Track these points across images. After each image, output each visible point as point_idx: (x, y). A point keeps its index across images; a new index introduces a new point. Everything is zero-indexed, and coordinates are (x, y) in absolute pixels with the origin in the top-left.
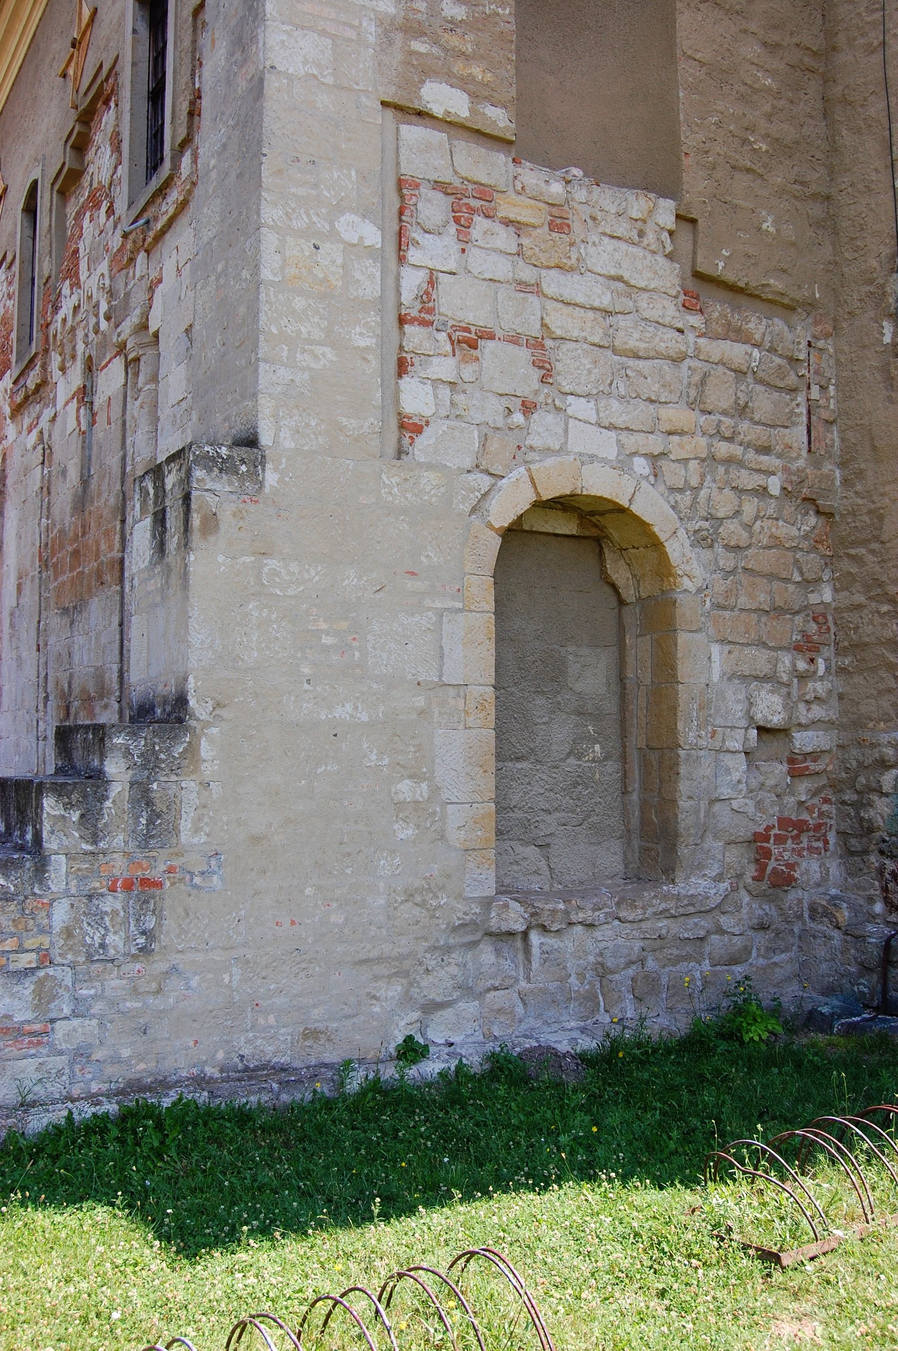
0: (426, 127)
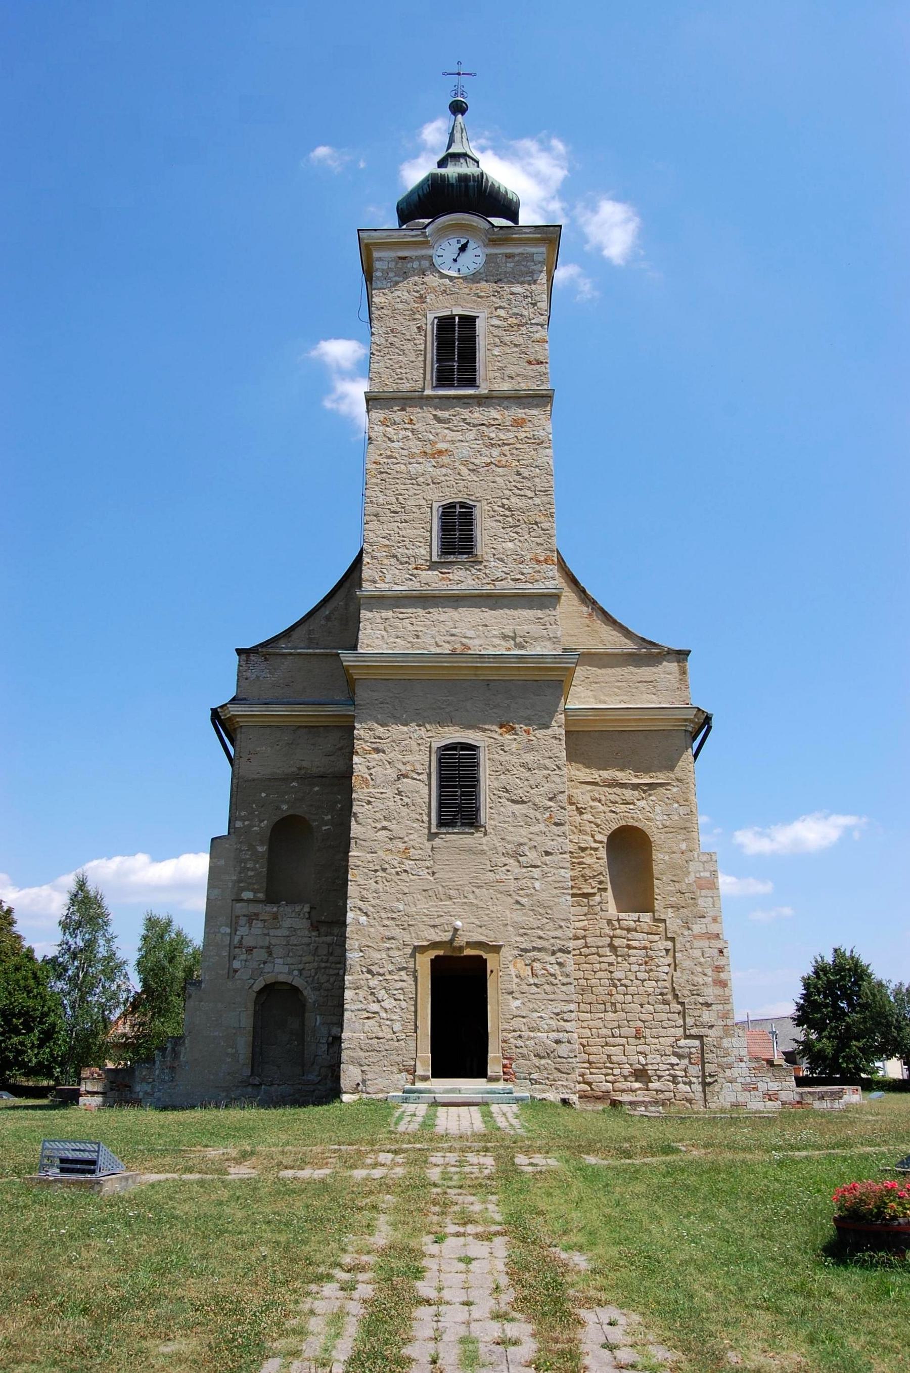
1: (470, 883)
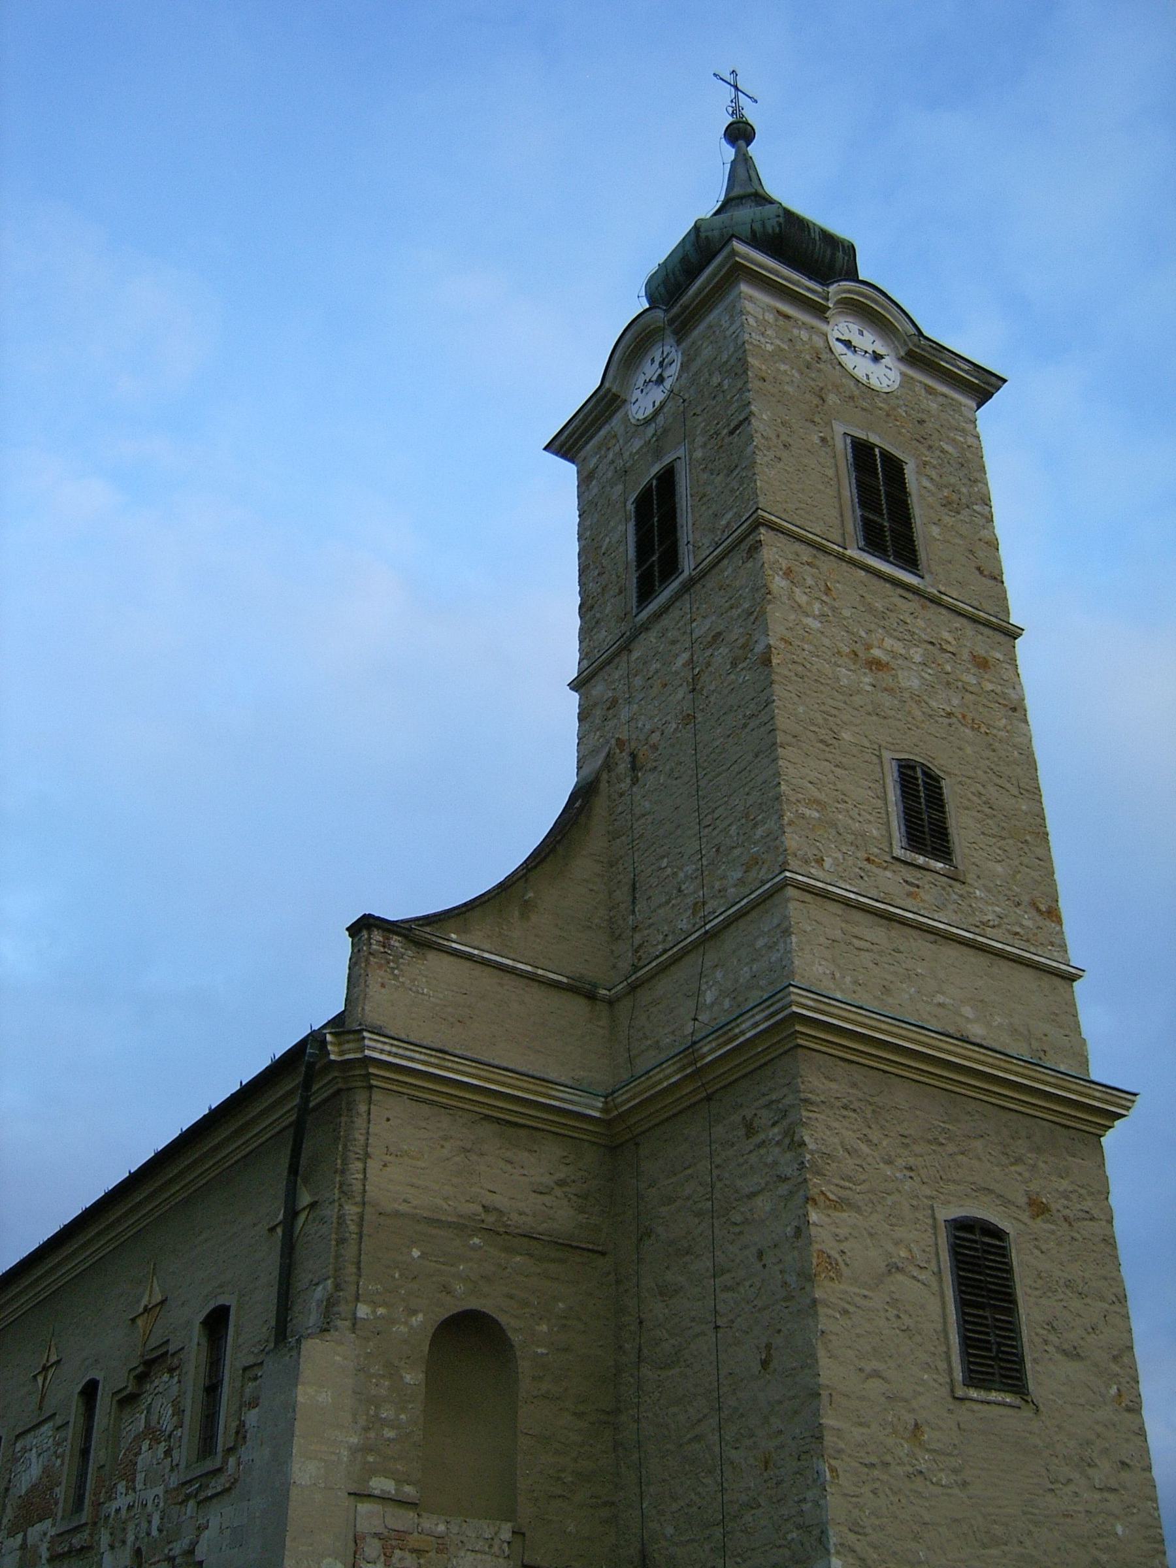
0: (370, 1502)
1: (1025, 1513)
